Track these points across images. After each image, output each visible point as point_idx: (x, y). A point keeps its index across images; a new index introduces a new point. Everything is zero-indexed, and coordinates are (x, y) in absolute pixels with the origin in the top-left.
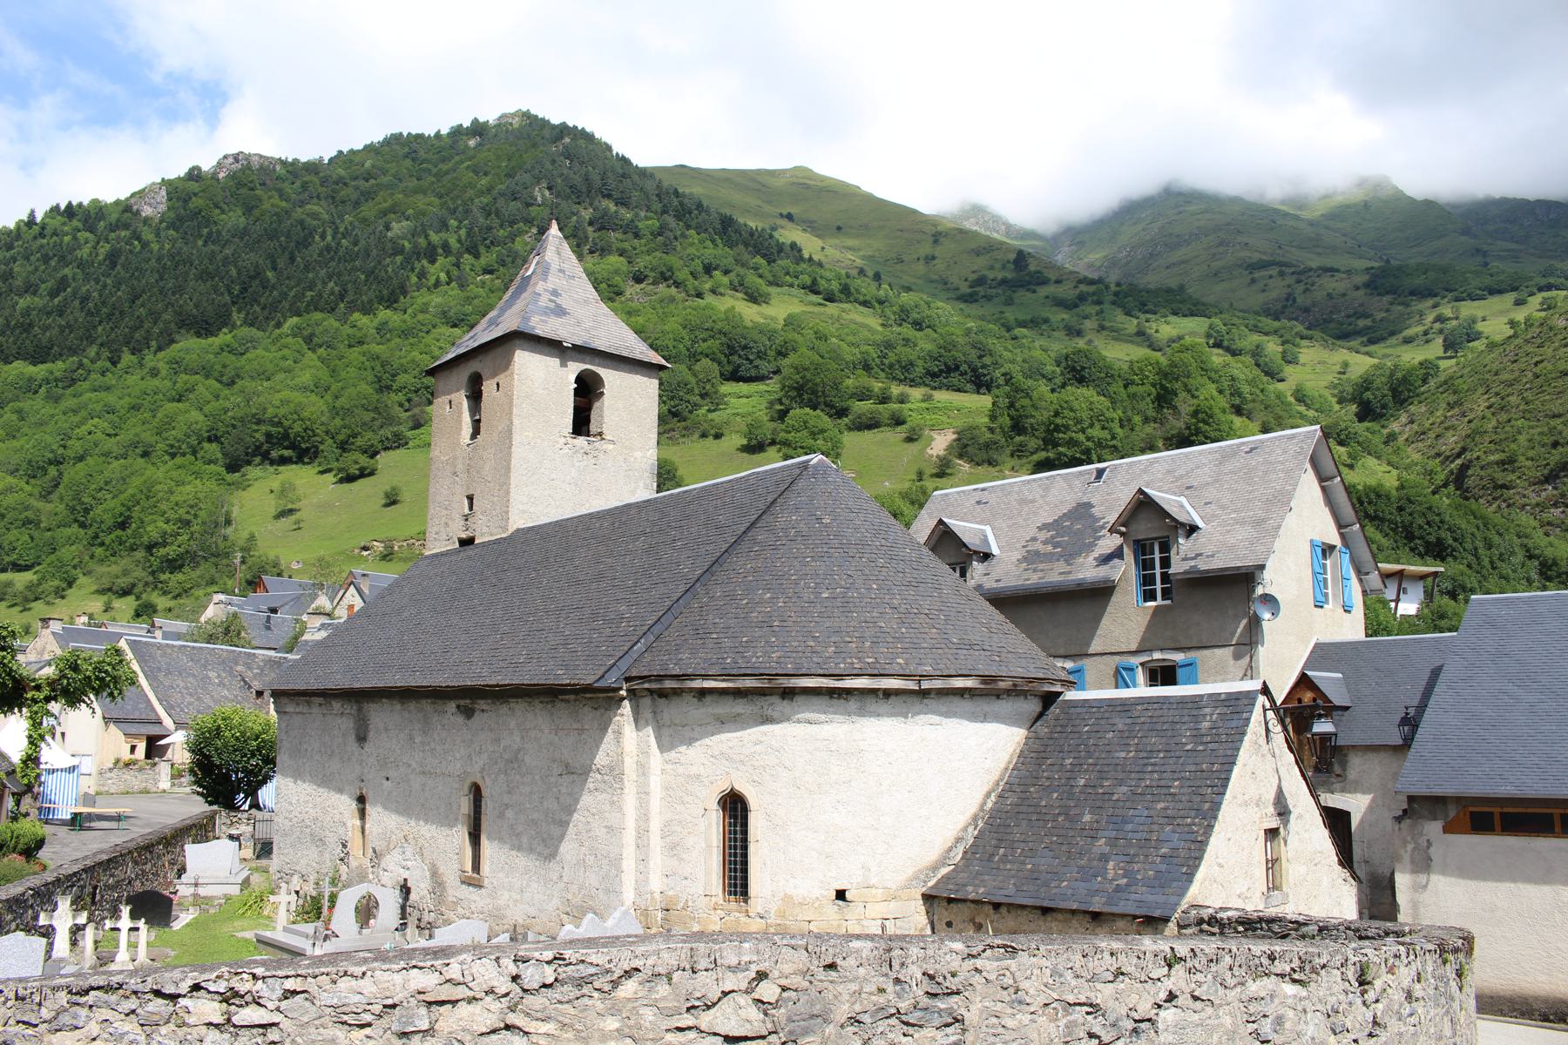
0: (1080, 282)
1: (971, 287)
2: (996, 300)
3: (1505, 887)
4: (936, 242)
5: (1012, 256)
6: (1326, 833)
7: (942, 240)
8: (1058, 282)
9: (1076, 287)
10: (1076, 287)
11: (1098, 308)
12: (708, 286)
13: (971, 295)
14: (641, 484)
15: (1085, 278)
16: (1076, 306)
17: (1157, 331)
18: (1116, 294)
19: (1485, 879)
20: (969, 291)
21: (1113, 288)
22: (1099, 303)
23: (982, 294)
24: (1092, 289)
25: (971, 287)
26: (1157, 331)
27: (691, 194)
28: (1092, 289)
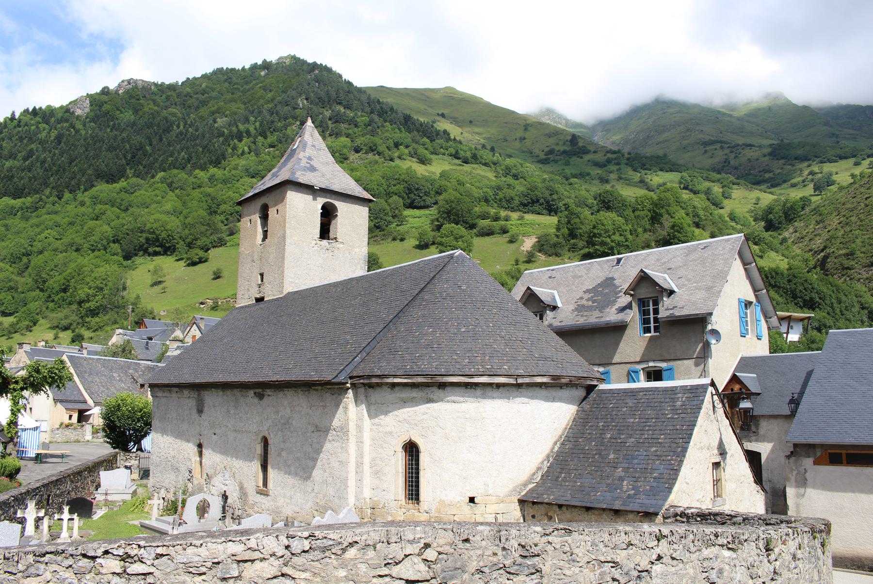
0: (608, 152)
2: (560, 163)
4: (526, 129)
5: (569, 138)
8: (595, 152)
9: (605, 155)
10: (605, 155)
11: (618, 167)
13: (546, 160)
15: (611, 150)
16: (605, 166)
17: (651, 180)
18: (628, 159)
20: (545, 157)
21: (626, 155)
24: (614, 156)
25: (546, 155)
26: (651, 180)
28: (614, 156)
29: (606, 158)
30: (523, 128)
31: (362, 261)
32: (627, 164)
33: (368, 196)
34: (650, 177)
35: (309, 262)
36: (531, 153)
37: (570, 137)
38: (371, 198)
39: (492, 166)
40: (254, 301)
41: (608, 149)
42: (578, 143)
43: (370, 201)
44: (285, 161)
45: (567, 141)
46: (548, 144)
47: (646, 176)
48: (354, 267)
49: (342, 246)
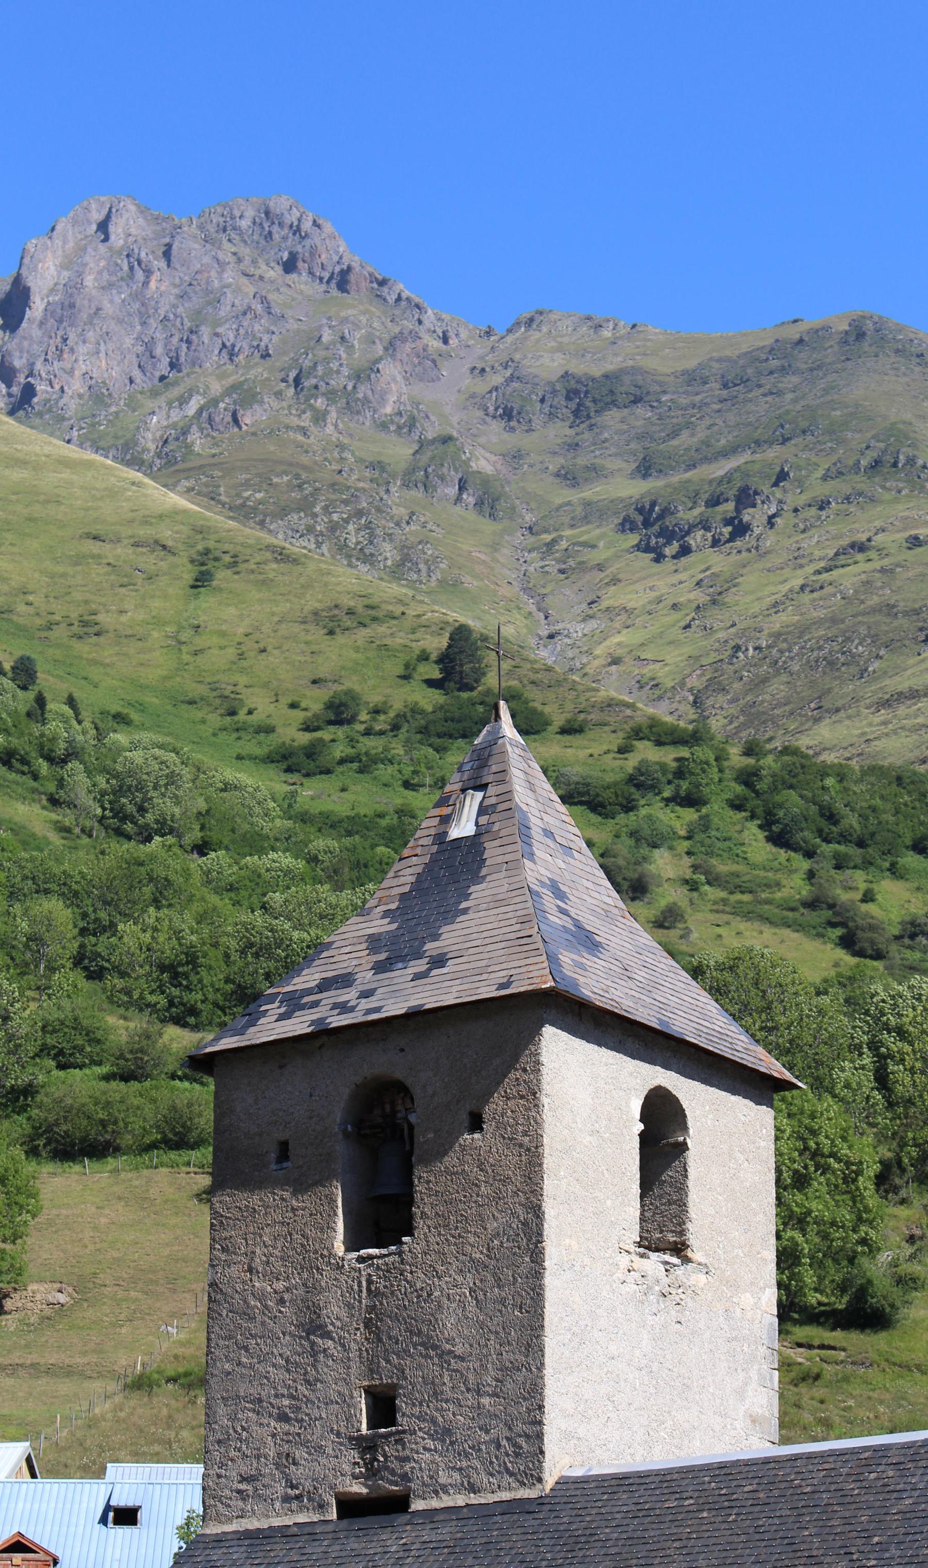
0: (637, 734)
1: (307, 728)
2: (385, 772)
3: (724, 1093)
4: (201, 581)
5: (438, 643)
6: (604, 1051)
7: (222, 576)
8: (569, 730)
9: (623, 750)
10: (623, 750)
11: (690, 815)
12: (212, 952)
13: (311, 752)
14: (754, 1375)
15: (654, 723)
16: (629, 807)
17: (868, 897)
18: (748, 778)
19: (693, 1079)
20: (305, 738)
21: (736, 758)
22: (691, 801)
23: (339, 751)
24: (668, 756)
25: (307, 728)
26: (868, 897)
27: (891, 765)
28: (668, 756)
29: (631, 763)
30: (188, 574)
31: (763, 1350)
32: (737, 805)
33: (775, 1068)
34: (860, 878)
35: (613, 1349)
36: (232, 713)
37: (443, 642)
38: (788, 1076)
39: (43, 767)
40: (333, 1514)
41: (639, 719)
42: (480, 674)
43: (781, 1085)
44: (419, 886)
45: (424, 657)
46: (323, 671)
47: (839, 876)
48: (742, 1375)
49: (702, 1278)
